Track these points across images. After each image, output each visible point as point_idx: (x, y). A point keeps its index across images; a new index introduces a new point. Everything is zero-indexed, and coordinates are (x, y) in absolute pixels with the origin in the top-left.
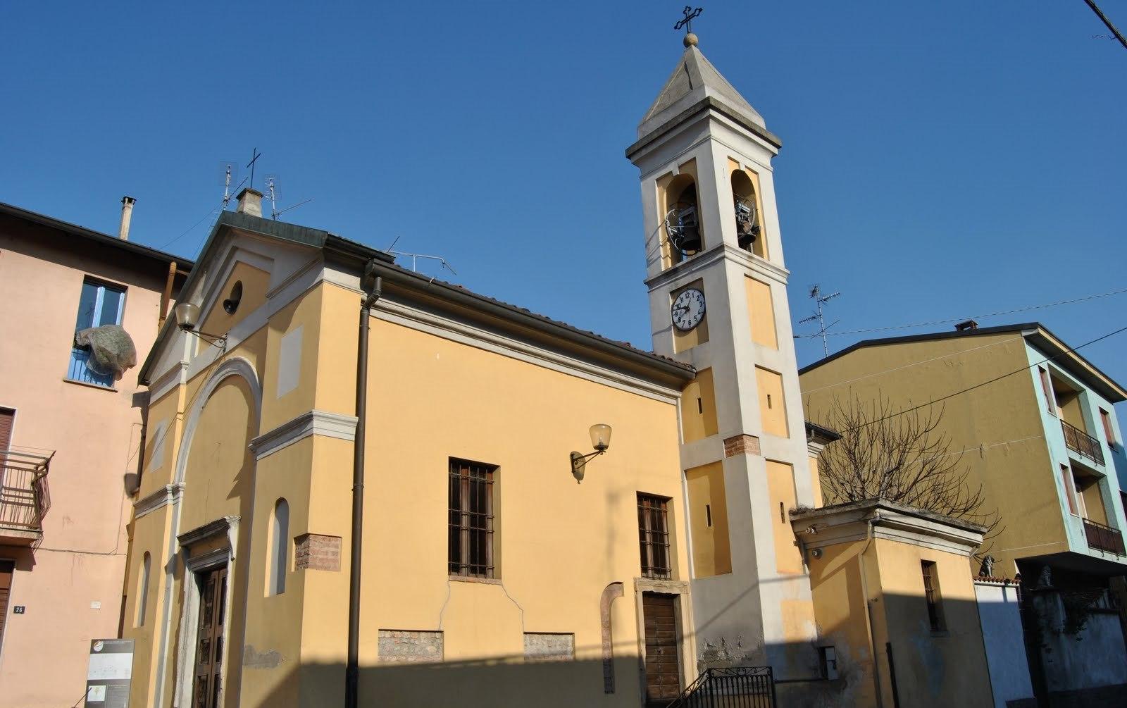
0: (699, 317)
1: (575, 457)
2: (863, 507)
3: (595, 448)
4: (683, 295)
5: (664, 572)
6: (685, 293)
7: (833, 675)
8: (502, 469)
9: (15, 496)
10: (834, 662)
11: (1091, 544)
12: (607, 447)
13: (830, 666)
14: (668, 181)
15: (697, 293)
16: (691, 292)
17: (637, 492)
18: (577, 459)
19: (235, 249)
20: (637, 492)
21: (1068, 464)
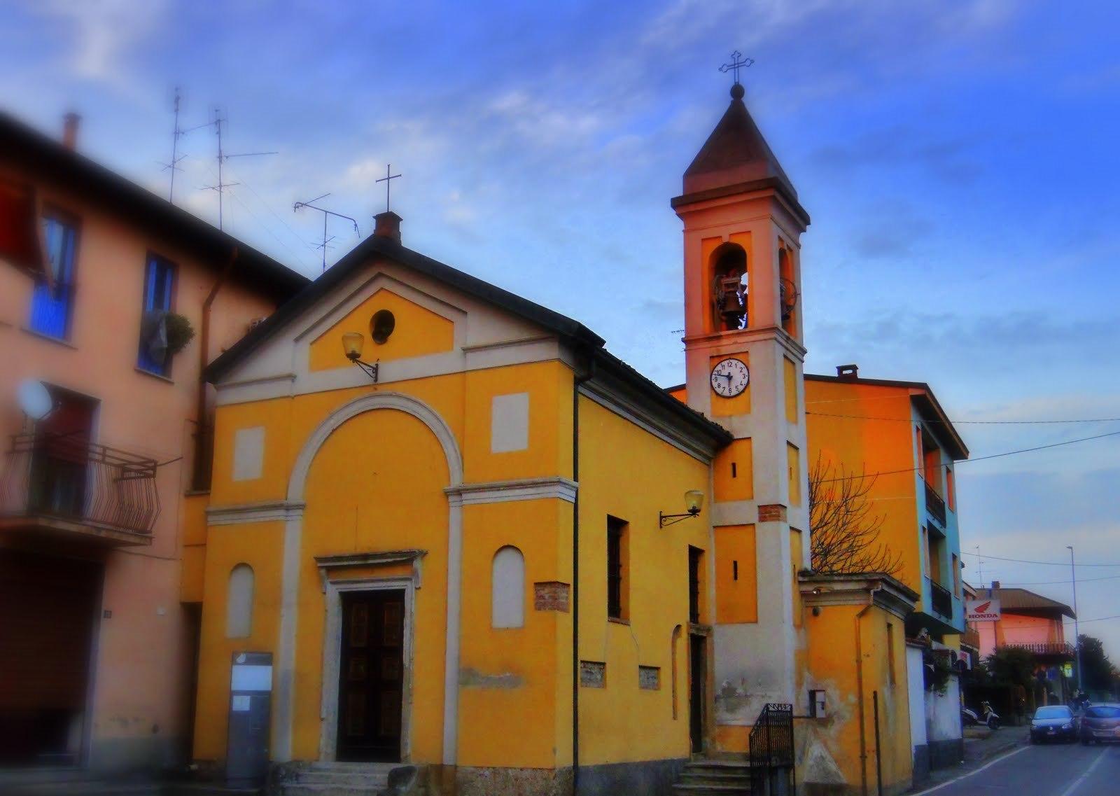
0: (741, 388)
1: (663, 514)
2: (869, 578)
3: (689, 511)
4: (725, 363)
5: (618, 616)
6: (728, 361)
7: (820, 714)
8: (631, 525)
9: (254, 518)
10: (823, 704)
11: (934, 609)
12: (699, 511)
13: (818, 706)
14: (714, 245)
15: (740, 365)
16: (734, 362)
17: (690, 546)
18: (665, 517)
19: (380, 275)
20: (690, 546)
21: (926, 527)
